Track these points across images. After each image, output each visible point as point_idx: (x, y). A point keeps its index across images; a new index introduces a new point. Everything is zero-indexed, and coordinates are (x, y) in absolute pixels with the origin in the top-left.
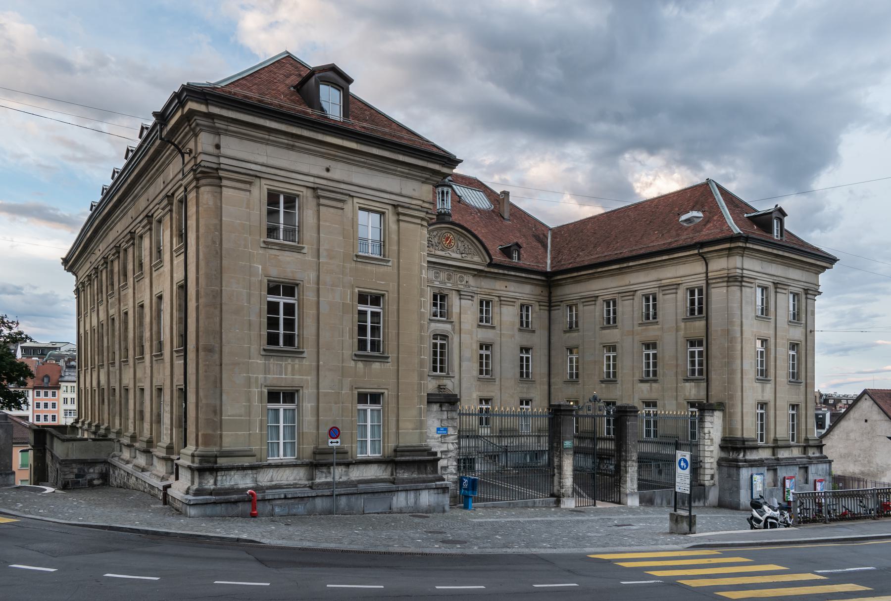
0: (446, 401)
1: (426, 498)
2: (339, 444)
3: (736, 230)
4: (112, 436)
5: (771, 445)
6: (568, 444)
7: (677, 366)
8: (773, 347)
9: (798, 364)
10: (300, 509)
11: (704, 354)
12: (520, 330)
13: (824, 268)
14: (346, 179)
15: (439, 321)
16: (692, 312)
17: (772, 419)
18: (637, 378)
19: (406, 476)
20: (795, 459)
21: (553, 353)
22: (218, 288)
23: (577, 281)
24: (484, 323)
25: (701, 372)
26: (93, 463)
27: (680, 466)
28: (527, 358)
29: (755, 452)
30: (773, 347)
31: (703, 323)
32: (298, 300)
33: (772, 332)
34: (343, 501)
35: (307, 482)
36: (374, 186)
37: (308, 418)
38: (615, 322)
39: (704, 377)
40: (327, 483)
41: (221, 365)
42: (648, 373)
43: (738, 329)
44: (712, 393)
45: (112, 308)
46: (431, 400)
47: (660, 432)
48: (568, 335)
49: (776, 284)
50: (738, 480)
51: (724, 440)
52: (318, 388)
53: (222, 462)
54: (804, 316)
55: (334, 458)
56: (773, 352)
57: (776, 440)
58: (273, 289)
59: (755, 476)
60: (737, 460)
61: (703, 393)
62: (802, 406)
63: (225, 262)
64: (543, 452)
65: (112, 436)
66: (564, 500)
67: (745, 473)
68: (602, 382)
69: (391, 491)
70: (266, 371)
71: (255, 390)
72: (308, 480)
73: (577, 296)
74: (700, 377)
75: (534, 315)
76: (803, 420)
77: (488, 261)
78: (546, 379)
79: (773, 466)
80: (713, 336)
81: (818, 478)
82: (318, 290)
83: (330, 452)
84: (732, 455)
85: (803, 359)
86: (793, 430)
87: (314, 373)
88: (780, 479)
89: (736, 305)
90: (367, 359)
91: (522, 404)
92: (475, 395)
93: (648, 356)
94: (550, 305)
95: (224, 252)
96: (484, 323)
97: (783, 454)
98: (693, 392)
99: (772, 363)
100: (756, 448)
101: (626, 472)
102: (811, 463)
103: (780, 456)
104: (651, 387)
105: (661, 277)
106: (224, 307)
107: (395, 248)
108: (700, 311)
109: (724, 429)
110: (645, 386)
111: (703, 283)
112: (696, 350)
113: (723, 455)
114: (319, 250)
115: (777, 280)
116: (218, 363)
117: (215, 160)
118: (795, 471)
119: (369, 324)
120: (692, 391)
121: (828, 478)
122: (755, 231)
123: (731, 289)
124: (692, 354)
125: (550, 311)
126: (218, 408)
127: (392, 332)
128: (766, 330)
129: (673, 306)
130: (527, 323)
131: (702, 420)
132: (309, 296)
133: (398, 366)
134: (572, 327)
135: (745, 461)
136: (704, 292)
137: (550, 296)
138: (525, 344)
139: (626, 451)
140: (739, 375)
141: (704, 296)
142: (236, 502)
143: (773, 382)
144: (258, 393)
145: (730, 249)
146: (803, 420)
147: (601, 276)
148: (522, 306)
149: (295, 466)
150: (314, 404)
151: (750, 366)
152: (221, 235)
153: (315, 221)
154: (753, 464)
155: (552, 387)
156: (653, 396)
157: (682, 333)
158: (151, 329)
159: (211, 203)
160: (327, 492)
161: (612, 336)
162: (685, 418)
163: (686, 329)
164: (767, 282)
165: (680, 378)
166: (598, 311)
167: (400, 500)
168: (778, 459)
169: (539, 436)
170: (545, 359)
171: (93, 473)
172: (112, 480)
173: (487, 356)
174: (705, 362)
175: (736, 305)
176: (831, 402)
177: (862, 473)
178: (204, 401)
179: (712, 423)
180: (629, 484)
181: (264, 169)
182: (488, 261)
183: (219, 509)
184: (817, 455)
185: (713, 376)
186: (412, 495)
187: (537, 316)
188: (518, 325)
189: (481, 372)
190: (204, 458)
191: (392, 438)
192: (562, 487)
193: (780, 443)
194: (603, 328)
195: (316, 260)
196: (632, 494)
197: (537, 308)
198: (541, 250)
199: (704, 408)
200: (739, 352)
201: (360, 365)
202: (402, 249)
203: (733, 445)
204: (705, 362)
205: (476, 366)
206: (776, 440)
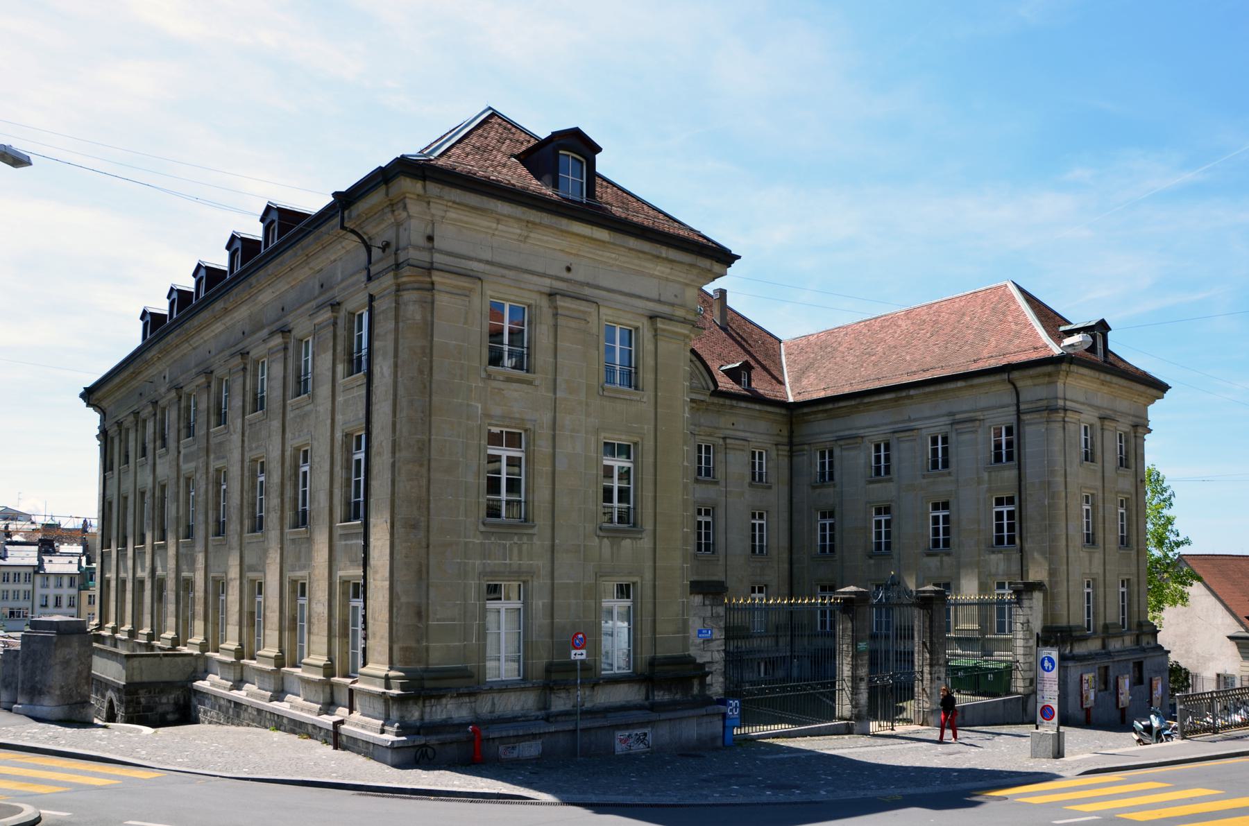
0: (711, 590)
2: (584, 657)
9: (1128, 525)
11: (1017, 515)
12: (751, 485)
22: (426, 438)
27: (1043, 668)
28: (761, 526)
30: (1101, 504)
31: (1015, 472)
32: (527, 452)
33: (1099, 484)
35: (538, 713)
41: (428, 546)
42: (936, 543)
43: (1060, 479)
45: (188, 458)
46: (697, 587)
48: (818, 491)
49: (1102, 419)
51: (1046, 629)
52: (553, 578)
54: (1133, 461)
56: (1101, 509)
57: (1106, 627)
58: (495, 439)
63: (435, 399)
71: (473, 583)
72: (540, 709)
73: (830, 437)
76: (1135, 599)
77: (712, 388)
78: (785, 555)
82: (554, 437)
85: (1134, 518)
86: (1089, 615)
87: (548, 555)
89: (1057, 448)
90: (613, 535)
93: (936, 519)
94: (793, 446)
95: (434, 386)
98: (1002, 567)
99: (1101, 525)
100: (1084, 639)
104: (941, 561)
106: (433, 464)
109: (1045, 616)
110: (933, 562)
111: (1011, 419)
112: (1005, 509)
114: (555, 380)
116: (424, 544)
119: (504, 477)
125: (791, 457)
126: (423, 608)
127: (648, 494)
129: (972, 451)
132: (543, 446)
133: (655, 544)
136: (1015, 432)
140: (1064, 542)
146: (1135, 599)
150: (547, 600)
152: (431, 362)
153: (552, 340)
155: (795, 566)
158: (282, 494)
159: (418, 317)
170: (784, 526)
173: (707, 524)
174: (1017, 526)
178: (404, 599)
179: (1031, 608)
182: (712, 388)
188: (748, 479)
195: (551, 395)
197: (774, 454)
202: (661, 378)
204: (1017, 526)
206: (1106, 627)
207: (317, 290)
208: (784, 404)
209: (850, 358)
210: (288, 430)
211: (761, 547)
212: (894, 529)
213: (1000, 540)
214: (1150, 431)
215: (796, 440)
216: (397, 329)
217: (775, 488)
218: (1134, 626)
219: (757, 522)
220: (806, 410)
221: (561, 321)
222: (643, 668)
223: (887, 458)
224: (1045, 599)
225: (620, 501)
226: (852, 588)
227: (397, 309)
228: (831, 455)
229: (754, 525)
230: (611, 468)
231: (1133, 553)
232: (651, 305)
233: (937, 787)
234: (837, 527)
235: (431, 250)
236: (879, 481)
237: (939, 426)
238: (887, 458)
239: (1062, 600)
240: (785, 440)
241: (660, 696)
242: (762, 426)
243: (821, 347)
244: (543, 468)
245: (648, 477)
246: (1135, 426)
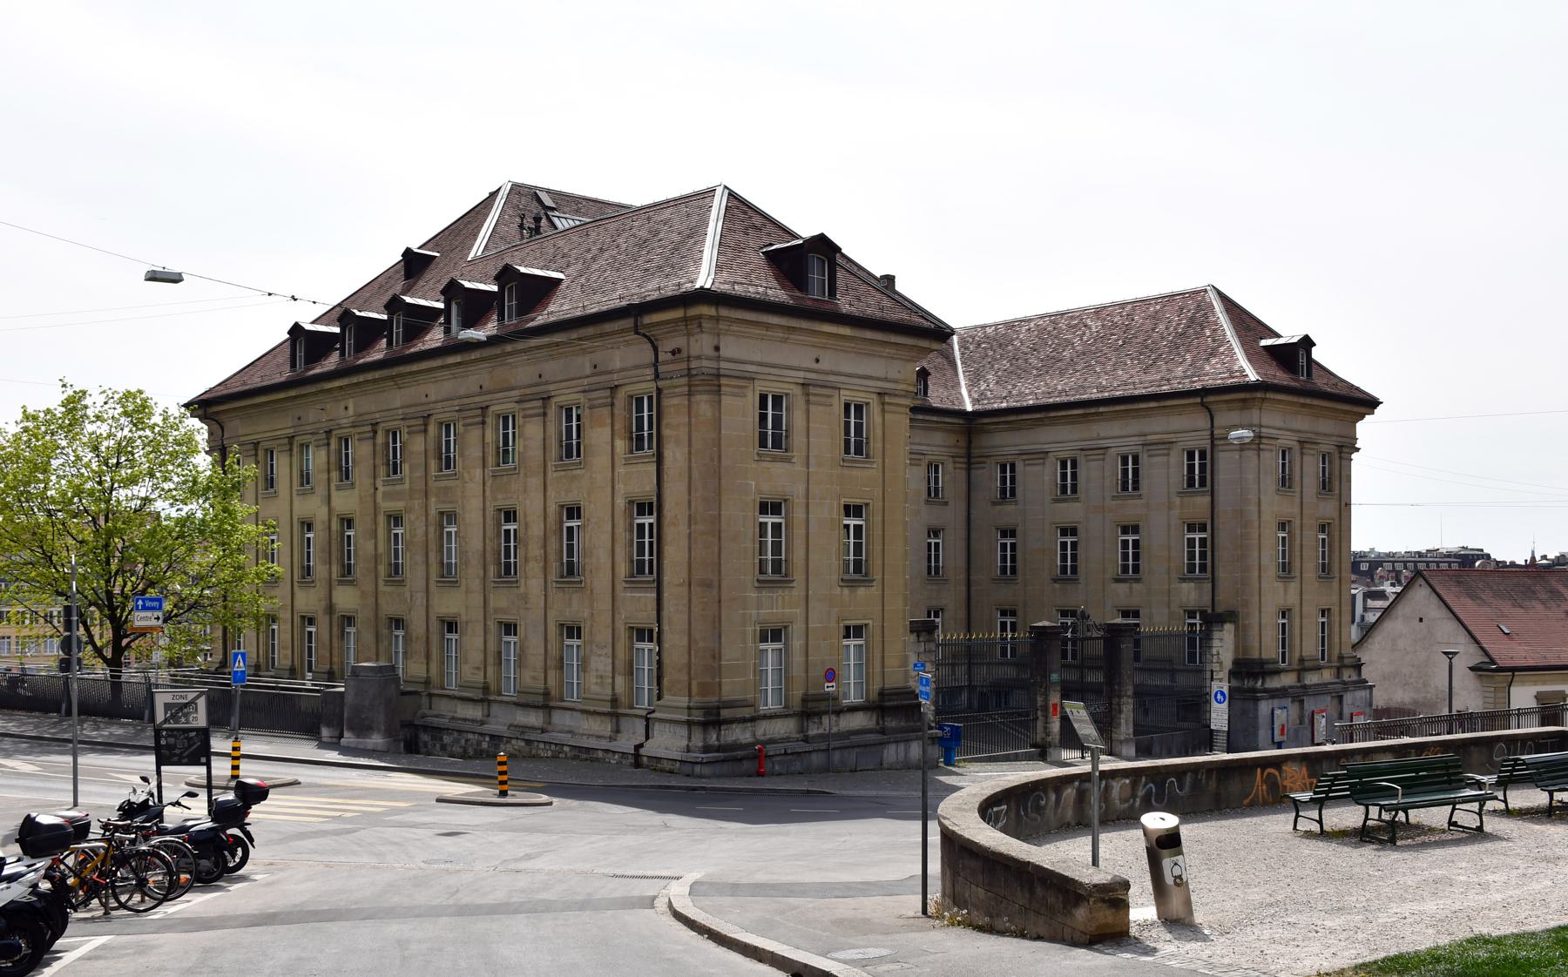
1: (915, 750)
3: (1253, 376)
5: (1295, 666)
6: (1055, 677)
7: (1169, 559)
8: (1298, 532)
10: (798, 766)
12: (927, 502)
13: (1362, 417)
14: (834, 369)
16: (1191, 483)
17: (1297, 631)
18: (1109, 575)
19: (894, 724)
20: (1326, 684)
21: (973, 536)
23: (1014, 427)
25: (1203, 568)
28: (937, 545)
29: (1276, 678)
30: (1298, 532)
31: (1208, 499)
32: (786, 518)
33: (1297, 510)
34: (836, 756)
36: (860, 372)
37: (798, 659)
38: (1074, 490)
39: (1209, 575)
40: (821, 736)
42: (1125, 569)
43: (1254, 508)
44: (1220, 597)
47: (1145, 654)
50: (1256, 717)
51: (1236, 662)
53: (725, 713)
55: (822, 706)
57: (1302, 660)
59: (1277, 712)
60: (1255, 690)
61: (1207, 598)
62: (1335, 609)
64: (961, 688)
66: (1051, 750)
67: (1264, 707)
68: (1055, 581)
69: (883, 744)
70: (759, 606)
71: (750, 629)
73: (1013, 450)
74: (1203, 575)
75: (947, 477)
76: (1336, 629)
78: (963, 577)
79: (1298, 695)
80: (1220, 521)
81: (1355, 711)
83: (826, 697)
84: (1248, 684)
88: (1307, 714)
89: (1251, 476)
93: (1125, 543)
94: (970, 460)
97: (1312, 679)
99: (1298, 554)
100: (1278, 672)
101: (1120, 712)
102: (1346, 690)
103: (1307, 682)
105: (1147, 429)
107: (880, 445)
108: (1202, 484)
110: (1122, 588)
111: (1206, 444)
112: (1197, 536)
113: (1235, 683)
115: (1303, 437)
117: (714, 364)
118: (1327, 702)
120: (1190, 594)
121: (1368, 710)
122: (1281, 377)
124: (1191, 542)
125: (969, 470)
127: (878, 548)
128: (1289, 509)
130: (936, 490)
131: (1207, 637)
132: (799, 514)
135: (1265, 691)
137: (969, 448)
138: (935, 523)
139: (1119, 684)
141: (1208, 461)
142: (740, 760)
143: (1298, 580)
144: (751, 630)
145: (1244, 400)
146: (1336, 629)
147: (1054, 422)
148: (930, 465)
149: (787, 716)
151: (1269, 557)
154: (1275, 694)
156: (1133, 603)
157: (1177, 512)
159: (709, 414)
160: (823, 746)
161: (1071, 512)
162: (1180, 635)
163: (1182, 506)
164: (1288, 440)
165: (1174, 576)
166: (1048, 474)
167: (891, 753)
168: (1305, 687)
169: (953, 665)
170: (962, 545)
175: (1251, 476)
176: (1364, 567)
177: (1416, 702)
178: (701, 644)
180: (1123, 728)
181: (759, 369)
183: (726, 768)
184: (1355, 678)
185: (1222, 574)
186: (902, 747)
187: (951, 478)
188: (924, 495)
190: (707, 710)
191: (878, 679)
192: (1048, 734)
193: (1307, 664)
194: (1057, 501)
196: (1127, 741)
197: (950, 466)
198: (949, 373)
199: (1213, 619)
200: (1256, 541)
201: (846, 591)
203: (1248, 670)
206: (1302, 660)
207: (588, 371)
208: (962, 414)
209: (1033, 361)
210: (549, 488)
211: (937, 568)
212: (1080, 552)
213: (1191, 569)
214: (1358, 450)
215: (975, 452)
216: (690, 423)
217: (951, 503)
218: (1335, 658)
219: (933, 541)
220: (986, 420)
221: (812, 408)
222: (874, 696)
223: (1074, 475)
224: (1237, 630)
226: (1046, 623)
227: (689, 406)
228: (1013, 470)
231: (1335, 584)
232: (880, 384)
234: (1019, 548)
235: (718, 358)
236: (1065, 501)
237: (1130, 446)
238: (1074, 475)
239: (1254, 632)
240: (963, 452)
241: (891, 723)
242: (938, 438)
243: (998, 343)
244: (799, 532)
245: (878, 532)
246: (1340, 447)
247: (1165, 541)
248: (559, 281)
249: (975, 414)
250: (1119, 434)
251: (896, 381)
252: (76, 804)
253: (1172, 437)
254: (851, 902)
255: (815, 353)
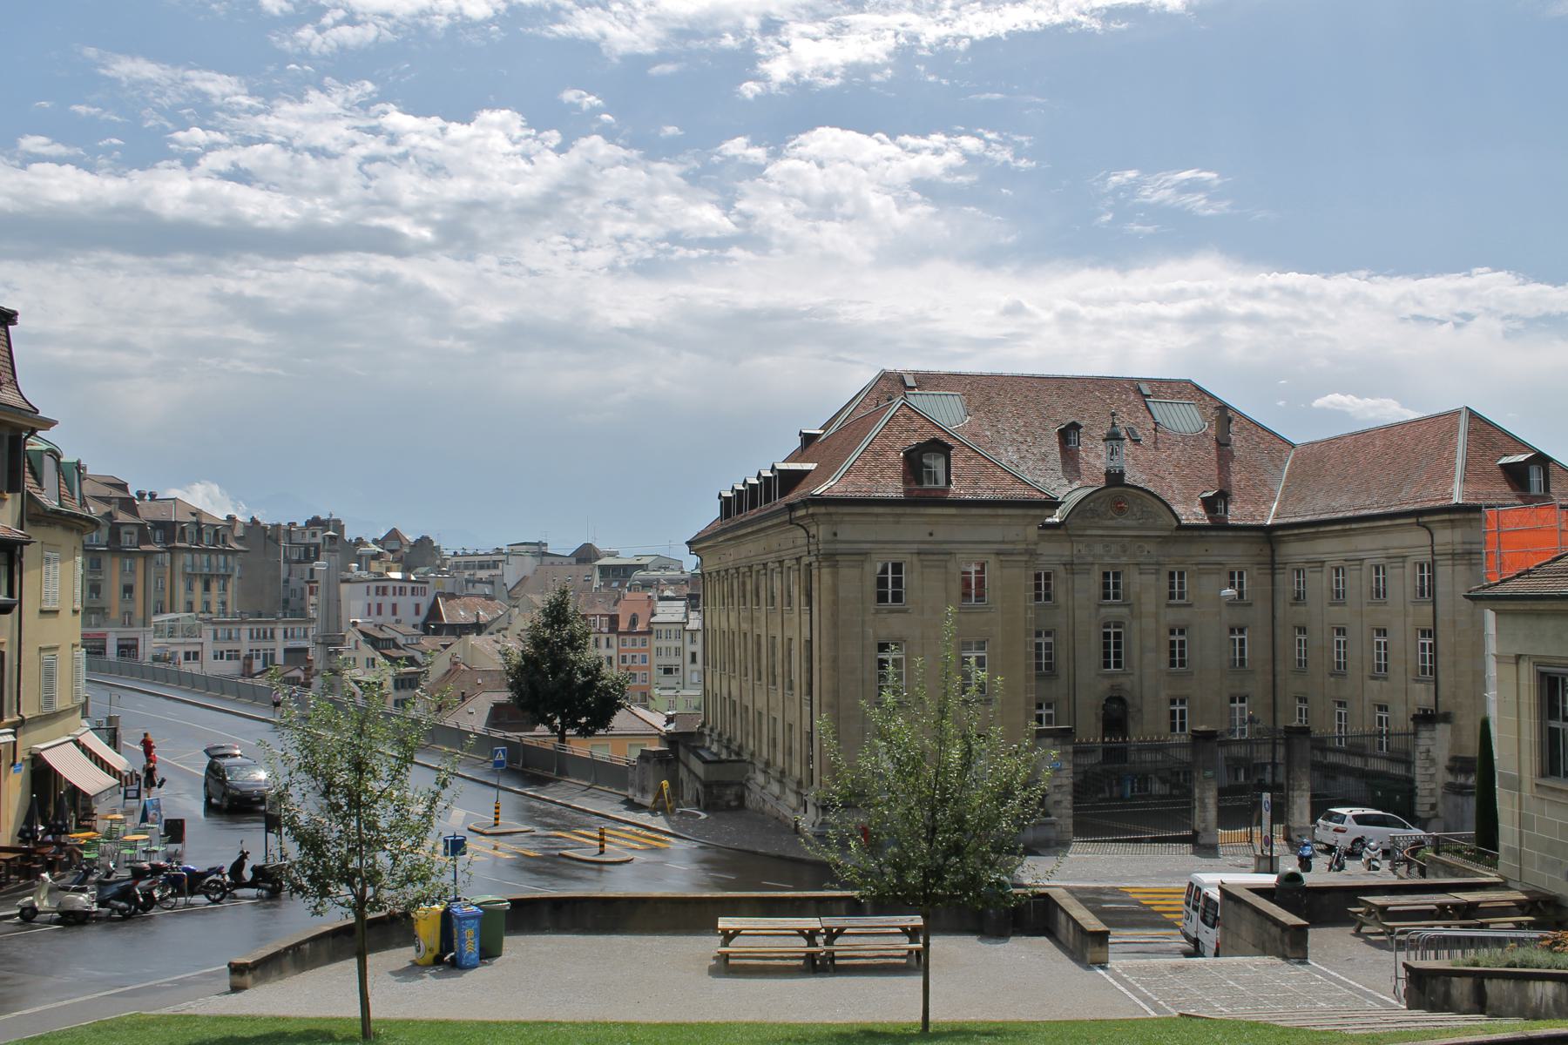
4: (746, 757)
15: (1111, 605)
23: (1302, 538)
24: (1176, 601)
26: (728, 785)
51: (1454, 759)
65: (746, 757)
78: (1269, 667)
91: (1233, 700)
92: (1164, 694)
96: (1176, 601)
110: (1376, 683)
111: (1428, 558)
113: (1450, 779)
120: (1422, 696)
123: (1457, 568)
129: (1402, 583)
134: (1299, 598)
137: (1273, 556)
147: (1325, 535)
157: (1410, 620)
165: (1410, 676)
171: (730, 793)
172: (747, 803)
179: (1432, 739)
189: (1172, 664)
197: (1255, 572)
205: (1166, 656)
215: (1278, 559)
225: (287, 651)
229: (1172, 643)
230: (287, 651)
233: (1127, 918)
240: (1268, 559)
242: (1239, 549)
243: (1320, 460)
247: (1405, 646)
248: (806, 473)
249: (1273, 527)
250: (1369, 545)
251: (1013, 542)
252: (602, 852)
253: (1404, 552)
254: (1471, 954)
255: (929, 529)
